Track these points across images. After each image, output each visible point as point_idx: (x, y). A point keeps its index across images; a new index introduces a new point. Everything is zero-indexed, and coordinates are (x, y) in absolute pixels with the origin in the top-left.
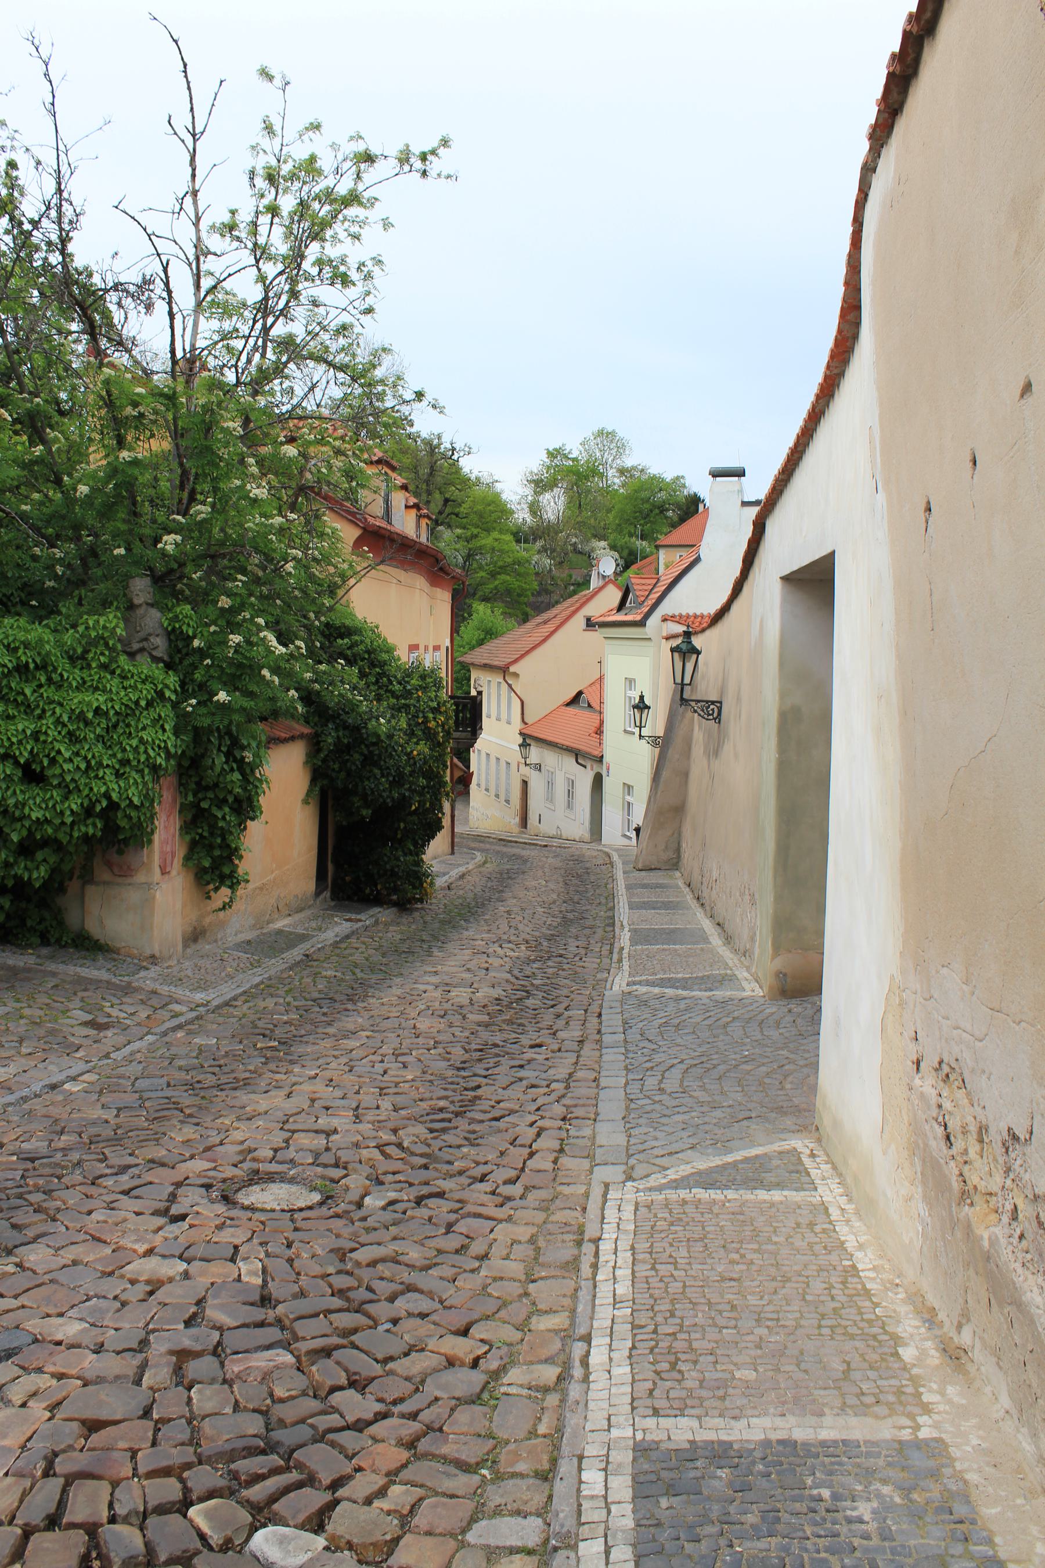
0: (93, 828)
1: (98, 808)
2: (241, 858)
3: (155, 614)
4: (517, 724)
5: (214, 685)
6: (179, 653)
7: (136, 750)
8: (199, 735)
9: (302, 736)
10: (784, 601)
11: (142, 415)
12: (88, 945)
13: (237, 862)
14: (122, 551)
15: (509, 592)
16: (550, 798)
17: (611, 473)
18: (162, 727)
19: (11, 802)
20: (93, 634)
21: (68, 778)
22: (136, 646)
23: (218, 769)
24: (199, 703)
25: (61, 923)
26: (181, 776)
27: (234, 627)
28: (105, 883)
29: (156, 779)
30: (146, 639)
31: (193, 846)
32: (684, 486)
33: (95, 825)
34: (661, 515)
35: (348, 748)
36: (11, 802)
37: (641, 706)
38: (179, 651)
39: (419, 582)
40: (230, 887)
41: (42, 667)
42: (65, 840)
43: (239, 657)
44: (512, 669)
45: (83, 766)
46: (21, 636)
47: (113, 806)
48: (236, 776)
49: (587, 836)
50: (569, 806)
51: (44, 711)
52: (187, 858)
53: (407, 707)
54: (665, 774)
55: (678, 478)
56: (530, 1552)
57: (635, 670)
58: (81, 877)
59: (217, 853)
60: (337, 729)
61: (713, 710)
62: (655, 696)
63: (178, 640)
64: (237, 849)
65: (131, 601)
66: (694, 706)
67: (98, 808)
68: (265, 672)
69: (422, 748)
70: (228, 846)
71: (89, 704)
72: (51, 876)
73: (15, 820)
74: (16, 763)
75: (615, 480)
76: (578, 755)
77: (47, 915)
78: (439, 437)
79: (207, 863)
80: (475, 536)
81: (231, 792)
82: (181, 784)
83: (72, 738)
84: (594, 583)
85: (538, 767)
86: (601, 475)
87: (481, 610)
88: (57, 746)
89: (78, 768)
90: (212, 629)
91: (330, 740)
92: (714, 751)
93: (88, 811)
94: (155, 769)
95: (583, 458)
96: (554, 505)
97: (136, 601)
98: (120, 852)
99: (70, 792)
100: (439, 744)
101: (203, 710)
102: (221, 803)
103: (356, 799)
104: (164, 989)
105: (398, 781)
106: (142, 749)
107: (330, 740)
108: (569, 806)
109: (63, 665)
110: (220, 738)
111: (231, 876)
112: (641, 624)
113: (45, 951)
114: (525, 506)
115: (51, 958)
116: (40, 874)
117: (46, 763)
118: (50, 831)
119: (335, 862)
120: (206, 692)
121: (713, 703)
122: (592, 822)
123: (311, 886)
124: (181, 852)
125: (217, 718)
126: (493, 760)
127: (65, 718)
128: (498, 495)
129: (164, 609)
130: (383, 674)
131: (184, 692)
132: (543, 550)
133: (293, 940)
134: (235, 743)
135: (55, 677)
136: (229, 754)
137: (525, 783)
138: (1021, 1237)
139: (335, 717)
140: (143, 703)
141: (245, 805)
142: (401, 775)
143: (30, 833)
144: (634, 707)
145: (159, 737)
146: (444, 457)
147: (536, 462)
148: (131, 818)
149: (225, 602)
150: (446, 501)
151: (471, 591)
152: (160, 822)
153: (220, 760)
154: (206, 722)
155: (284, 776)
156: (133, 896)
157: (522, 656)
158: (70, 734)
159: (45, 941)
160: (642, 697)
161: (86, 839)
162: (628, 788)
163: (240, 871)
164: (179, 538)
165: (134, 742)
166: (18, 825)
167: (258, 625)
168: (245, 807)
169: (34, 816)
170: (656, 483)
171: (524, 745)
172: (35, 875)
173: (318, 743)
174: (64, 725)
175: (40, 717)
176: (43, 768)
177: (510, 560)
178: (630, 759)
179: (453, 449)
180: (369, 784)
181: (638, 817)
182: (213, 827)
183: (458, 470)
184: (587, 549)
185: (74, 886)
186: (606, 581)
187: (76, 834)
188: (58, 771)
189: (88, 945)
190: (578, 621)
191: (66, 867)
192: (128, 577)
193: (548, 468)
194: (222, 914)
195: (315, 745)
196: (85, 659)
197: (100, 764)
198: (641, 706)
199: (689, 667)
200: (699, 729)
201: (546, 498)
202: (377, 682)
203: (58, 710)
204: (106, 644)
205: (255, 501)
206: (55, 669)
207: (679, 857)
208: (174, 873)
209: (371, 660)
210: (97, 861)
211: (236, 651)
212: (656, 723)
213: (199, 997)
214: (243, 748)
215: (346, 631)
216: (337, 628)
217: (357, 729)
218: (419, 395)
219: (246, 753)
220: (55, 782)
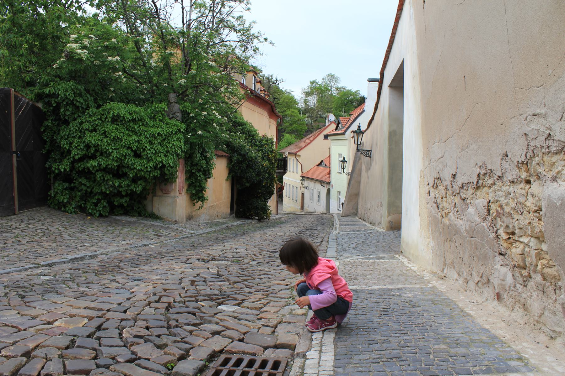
0: (157, 173)
1: (159, 166)
2: (205, 191)
3: (177, 105)
4: (300, 173)
5: (197, 129)
6: (185, 117)
7: (171, 147)
8: (192, 146)
9: (225, 156)
10: (390, 94)
11: (173, 39)
12: (154, 217)
13: (204, 192)
14: (166, 85)
15: (297, 130)
16: (312, 199)
17: (333, 89)
18: (180, 141)
19: (130, 163)
20: (157, 110)
21: (149, 156)
22: (171, 116)
23: (198, 158)
24: (192, 135)
25: (145, 210)
26: (186, 161)
27: (203, 109)
28: (160, 196)
29: (178, 159)
30: (174, 114)
31: (190, 186)
32: (359, 94)
33: (157, 173)
34: (351, 103)
35: (242, 162)
36: (130, 163)
37: (344, 161)
38: (185, 118)
39: (265, 114)
40: (202, 201)
41: (140, 120)
42: (148, 177)
43: (206, 119)
44: (298, 154)
45: (154, 152)
46: (133, 109)
47: (164, 166)
48: (204, 161)
49: (325, 211)
50: (319, 201)
51: (141, 134)
52: (187, 190)
53: (261, 150)
54: (352, 182)
55: (357, 91)
56: (302, 208)
57: (342, 149)
58: (152, 193)
59: (197, 189)
60: (237, 155)
61: (368, 153)
62: (349, 159)
63: (185, 114)
64: (204, 188)
65: (169, 101)
66: (363, 152)
67: (159, 166)
68: (214, 124)
69: (266, 164)
70: (201, 186)
71: (156, 131)
72: (143, 190)
73: (131, 170)
74: (132, 150)
75: (334, 92)
76: (321, 182)
77: (141, 206)
78: (272, 76)
79: (194, 192)
80: (285, 111)
81: (202, 167)
82: (185, 164)
83: (151, 143)
84: (327, 123)
85: (307, 188)
86: (330, 90)
87: (287, 136)
88: (145, 145)
89: (152, 153)
90: (197, 110)
91: (235, 158)
92: (369, 168)
93: (155, 168)
94: (178, 155)
95: (323, 84)
96: (313, 101)
97: (171, 101)
98: (165, 184)
99: (149, 161)
100: (273, 163)
101: (193, 137)
102: (200, 171)
103: (244, 180)
104: (180, 229)
105: (259, 174)
106: (173, 147)
107: (235, 158)
108: (319, 201)
109: (147, 119)
110: (199, 148)
111: (202, 197)
112: (344, 134)
113: (140, 218)
114: (302, 101)
115: (142, 219)
116: (139, 189)
117: (142, 150)
118: (143, 174)
119: (237, 204)
120: (194, 131)
121: (368, 151)
122: (327, 206)
123: (229, 211)
124: (185, 188)
125: (198, 140)
126: (291, 186)
127: (148, 136)
128: (293, 97)
129: (180, 104)
130: (253, 139)
131: (187, 131)
132: (309, 117)
133: (222, 224)
134: (204, 150)
135: (145, 123)
136: (202, 154)
137: (303, 194)
138: (457, 211)
139: (237, 151)
140: (174, 133)
141: (207, 172)
142: (259, 172)
143: (136, 174)
144: (341, 161)
145: (179, 144)
146: (273, 83)
147: (306, 85)
148: (169, 171)
149: (201, 101)
150: (274, 98)
151: (283, 130)
152: (179, 174)
153: (199, 155)
154: (195, 141)
155: (220, 169)
156: (169, 200)
157: (302, 149)
158: (150, 141)
159: (140, 215)
160: (344, 158)
161: (155, 177)
162: (339, 193)
163: (205, 196)
164: (185, 81)
165: (171, 145)
166: (132, 171)
167: (212, 109)
168: (207, 174)
169: (137, 168)
170: (349, 93)
171: (302, 180)
172: (137, 189)
173: (231, 160)
174: (148, 138)
175: (140, 136)
176: (141, 152)
177: (297, 119)
178: (340, 182)
179: (277, 80)
180: (249, 175)
181: (343, 200)
182: (196, 179)
183: (278, 88)
184: (325, 116)
185: (149, 198)
186: (331, 122)
187: (151, 175)
188: (146, 153)
189: (154, 217)
190: (322, 136)
191: (148, 187)
192: (168, 93)
193: (311, 88)
194: (199, 211)
195: (230, 160)
196: (154, 118)
197: (159, 152)
198: (344, 161)
199: (360, 138)
200: (364, 159)
201: (310, 98)
202: (251, 142)
203: (146, 133)
204: (161, 113)
205: (211, 66)
206: (145, 121)
207: (357, 211)
208: (183, 194)
209: (250, 135)
210: (157, 188)
211: (205, 117)
212: (349, 167)
213: (192, 232)
214: (206, 152)
215: (241, 124)
216: (238, 123)
217: (244, 155)
218: (266, 39)
219: (207, 154)
220: (145, 157)
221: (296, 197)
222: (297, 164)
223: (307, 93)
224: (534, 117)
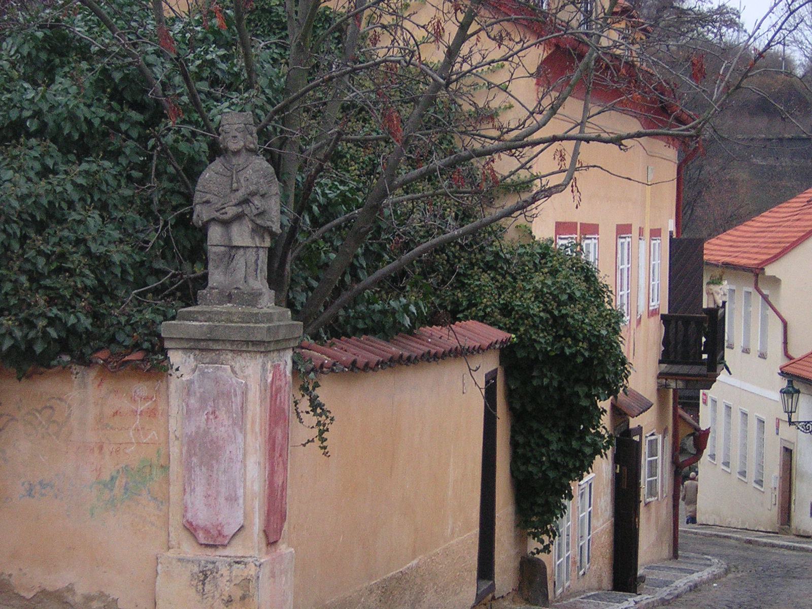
4: (777, 359)
126: (737, 417)
137: (788, 453)
171: (790, 392)
221: (760, 466)
222: (764, 318)
223: (373, 370)
224: (114, 410)
